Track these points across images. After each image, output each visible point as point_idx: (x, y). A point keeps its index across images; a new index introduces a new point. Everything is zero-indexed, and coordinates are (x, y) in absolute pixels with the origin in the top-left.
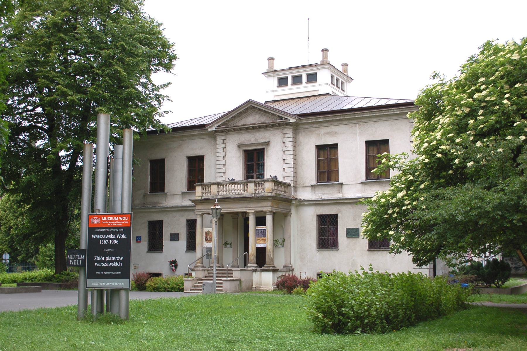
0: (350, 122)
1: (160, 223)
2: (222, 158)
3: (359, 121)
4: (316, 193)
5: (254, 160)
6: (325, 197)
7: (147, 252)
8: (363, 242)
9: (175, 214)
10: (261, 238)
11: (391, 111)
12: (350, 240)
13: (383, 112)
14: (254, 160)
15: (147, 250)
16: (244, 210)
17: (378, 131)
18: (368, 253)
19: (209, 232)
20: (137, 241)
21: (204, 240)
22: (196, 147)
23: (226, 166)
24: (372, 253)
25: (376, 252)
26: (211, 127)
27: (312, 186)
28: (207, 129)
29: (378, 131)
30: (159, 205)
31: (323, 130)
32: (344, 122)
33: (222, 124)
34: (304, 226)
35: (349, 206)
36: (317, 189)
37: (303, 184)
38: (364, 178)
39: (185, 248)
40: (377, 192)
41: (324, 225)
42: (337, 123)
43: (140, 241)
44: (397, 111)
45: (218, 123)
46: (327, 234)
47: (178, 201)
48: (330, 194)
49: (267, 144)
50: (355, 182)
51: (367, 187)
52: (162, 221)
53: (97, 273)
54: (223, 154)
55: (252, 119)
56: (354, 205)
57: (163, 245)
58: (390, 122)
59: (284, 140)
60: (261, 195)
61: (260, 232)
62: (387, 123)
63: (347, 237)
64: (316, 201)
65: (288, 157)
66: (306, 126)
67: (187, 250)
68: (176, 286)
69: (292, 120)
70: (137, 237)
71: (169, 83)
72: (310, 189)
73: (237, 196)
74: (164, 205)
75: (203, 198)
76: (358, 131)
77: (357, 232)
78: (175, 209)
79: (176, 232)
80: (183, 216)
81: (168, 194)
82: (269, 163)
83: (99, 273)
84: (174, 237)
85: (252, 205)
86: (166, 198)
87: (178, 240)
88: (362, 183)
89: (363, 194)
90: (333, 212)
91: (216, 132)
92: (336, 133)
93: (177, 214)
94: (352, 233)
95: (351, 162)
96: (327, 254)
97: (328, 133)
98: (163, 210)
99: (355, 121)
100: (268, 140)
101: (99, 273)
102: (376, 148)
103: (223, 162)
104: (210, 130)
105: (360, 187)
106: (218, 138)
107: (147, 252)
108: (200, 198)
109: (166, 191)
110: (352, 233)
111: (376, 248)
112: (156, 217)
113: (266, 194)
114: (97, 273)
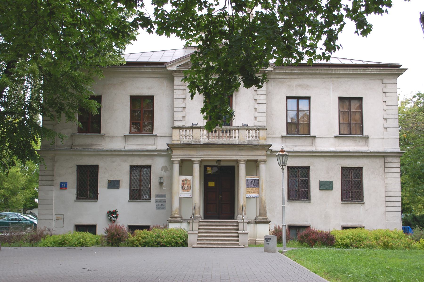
0: (324, 77)
1: (95, 169)
3: (333, 77)
4: (287, 144)
6: (296, 149)
7: (75, 201)
9: (114, 159)
10: (251, 189)
11: (369, 71)
13: (361, 71)
15: (75, 199)
16: (234, 158)
17: (352, 88)
18: (341, 205)
19: (186, 180)
20: (61, 188)
21: (181, 189)
22: (143, 87)
23: (186, 109)
24: (346, 206)
25: (349, 205)
26: (171, 66)
28: (166, 68)
29: (352, 88)
30: (93, 148)
31: (295, 82)
32: (317, 76)
33: (183, 65)
34: (274, 178)
35: (322, 159)
36: (288, 140)
37: (273, 134)
38: (337, 134)
39: (74, 196)
41: (358, 178)
42: (310, 76)
43: (66, 188)
44: (374, 71)
45: (180, 62)
46: (299, 185)
47: (118, 145)
48: (302, 146)
50: (328, 136)
51: (341, 141)
52: (97, 166)
56: (328, 159)
57: (98, 193)
58: (364, 81)
59: (385, 90)
60: (254, 143)
61: (250, 181)
63: (320, 190)
65: (261, 106)
66: (277, 76)
67: (130, 199)
68: (173, 240)
71: (388, 13)
72: (280, 140)
73: (225, 143)
74: (99, 148)
75: (182, 142)
76: (331, 87)
77: (331, 185)
78: (134, 153)
79: (116, 179)
80: (125, 161)
81: (106, 135)
84: (114, 184)
85: (243, 153)
87: (118, 187)
88: (336, 137)
89: (337, 148)
91: (175, 71)
92: (308, 86)
93: (118, 160)
94: (326, 186)
95: (325, 118)
97: (300, 86)
98: (100, 153)
99: (329, 76)
103: (183, 105)
104: (169, 69)
105: (333, 141)
106: (176, 79)
107: (75, 201)
108: (178, 142)
109: (102, 132)
110: (326, 186)
111: (349, 201)
112: (88, 161)
113: (261, 143)
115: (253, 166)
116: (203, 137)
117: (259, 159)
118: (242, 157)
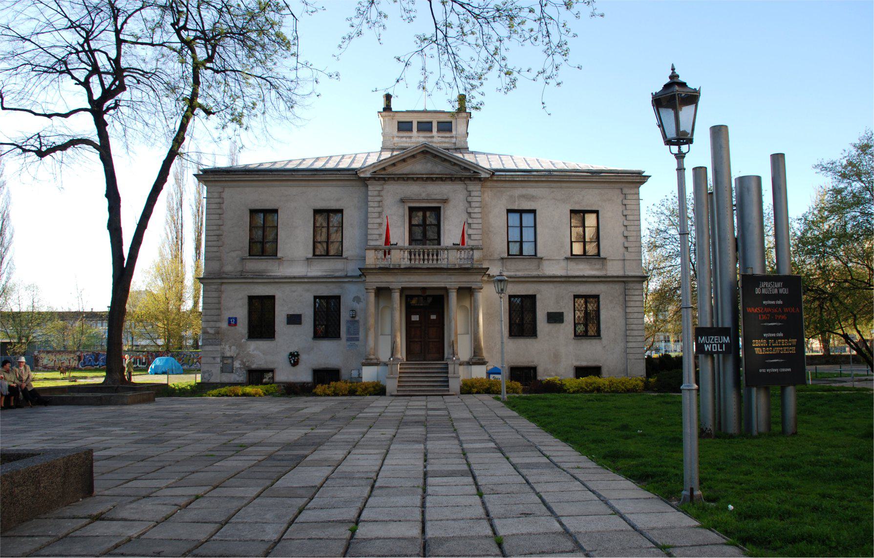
2: (377, 215)
5: (425, 223)
8: (567, 327)
12: (551, 326)
14: (425, 223)
24: (579, 341)
27: (502, 259)
35: (551, 286)
40: (319, 269)
43: (236, 324)
49: (445, 201)
53: (789, 370)
54: (379, 209)
55: (419, 167)
62: (596, 191)
64: (618, 277)
69: (483, 175)
70: (230, 318)
82: (447, 227)
83: (764, 371)
86: (279, 265)
88: (567, 259)
90: (531, 293)
96: (523, 344)
100: (445, 197)
101: (764, 371)
102: (326, 216)
105: (564, 264)
106: (370, 188)
109: (279, 255)
114: (789, 370)
115: (467, 292)
116: (399, 258)
117: (473, 287)
118: (451, 282)
